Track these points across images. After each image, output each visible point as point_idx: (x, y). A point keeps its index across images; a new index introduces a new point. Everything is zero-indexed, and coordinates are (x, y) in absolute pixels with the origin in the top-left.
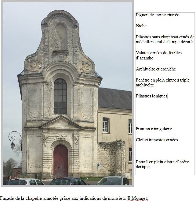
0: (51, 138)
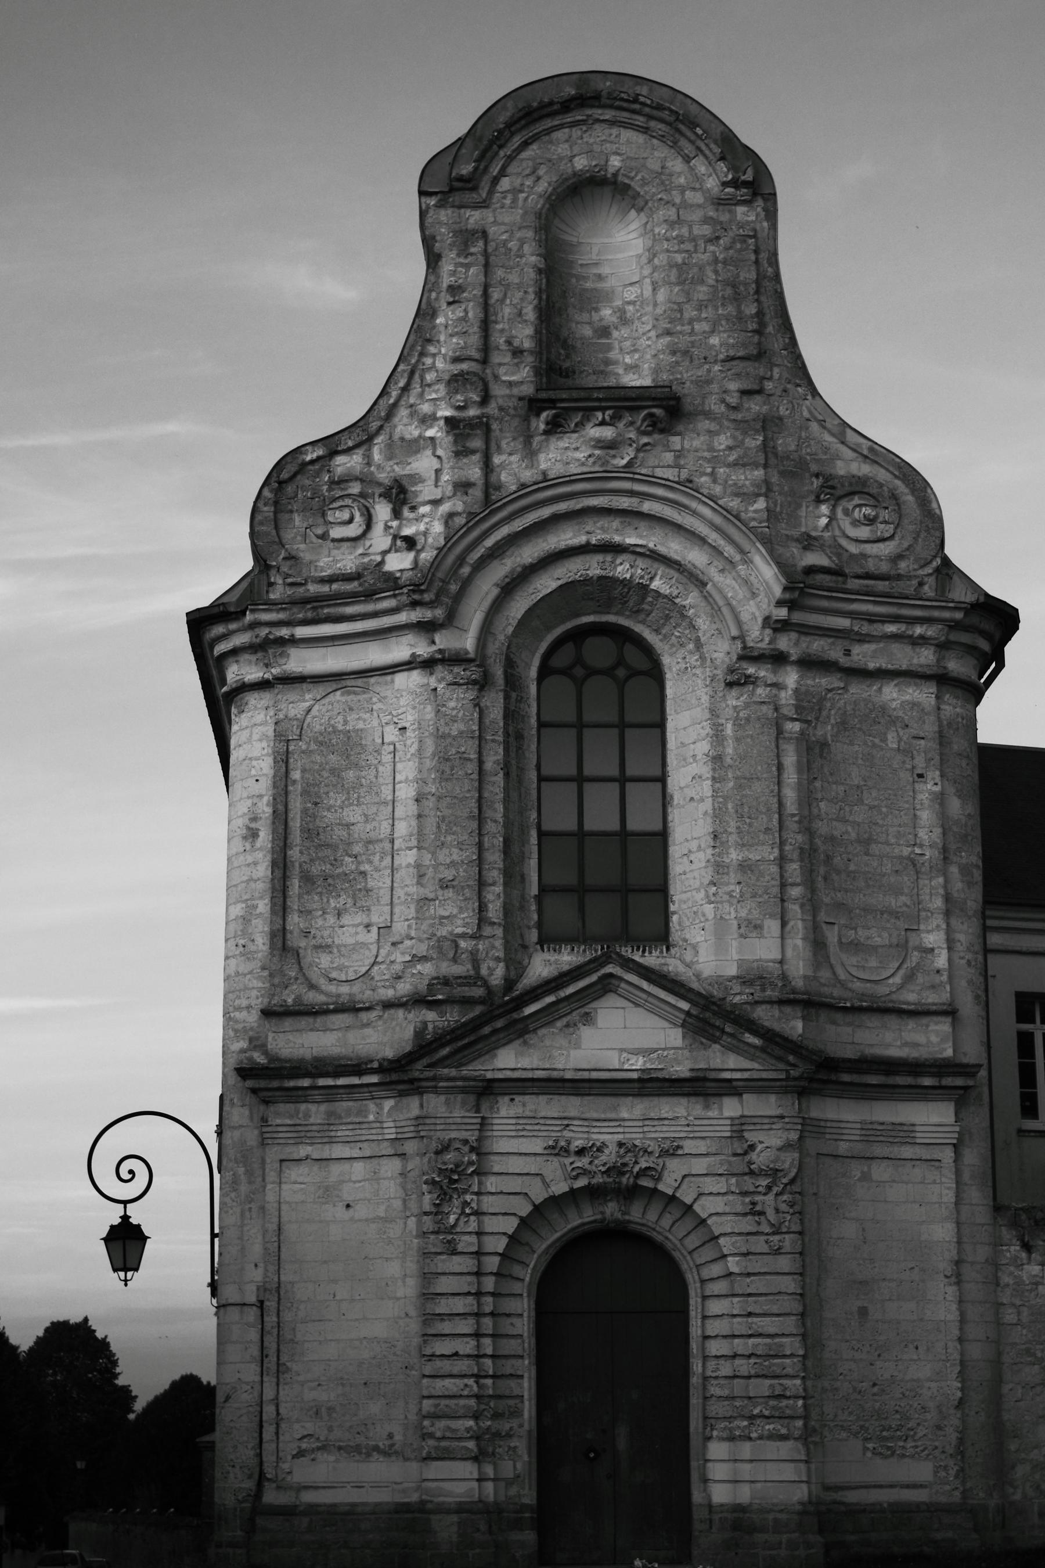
0: (516, 1165)
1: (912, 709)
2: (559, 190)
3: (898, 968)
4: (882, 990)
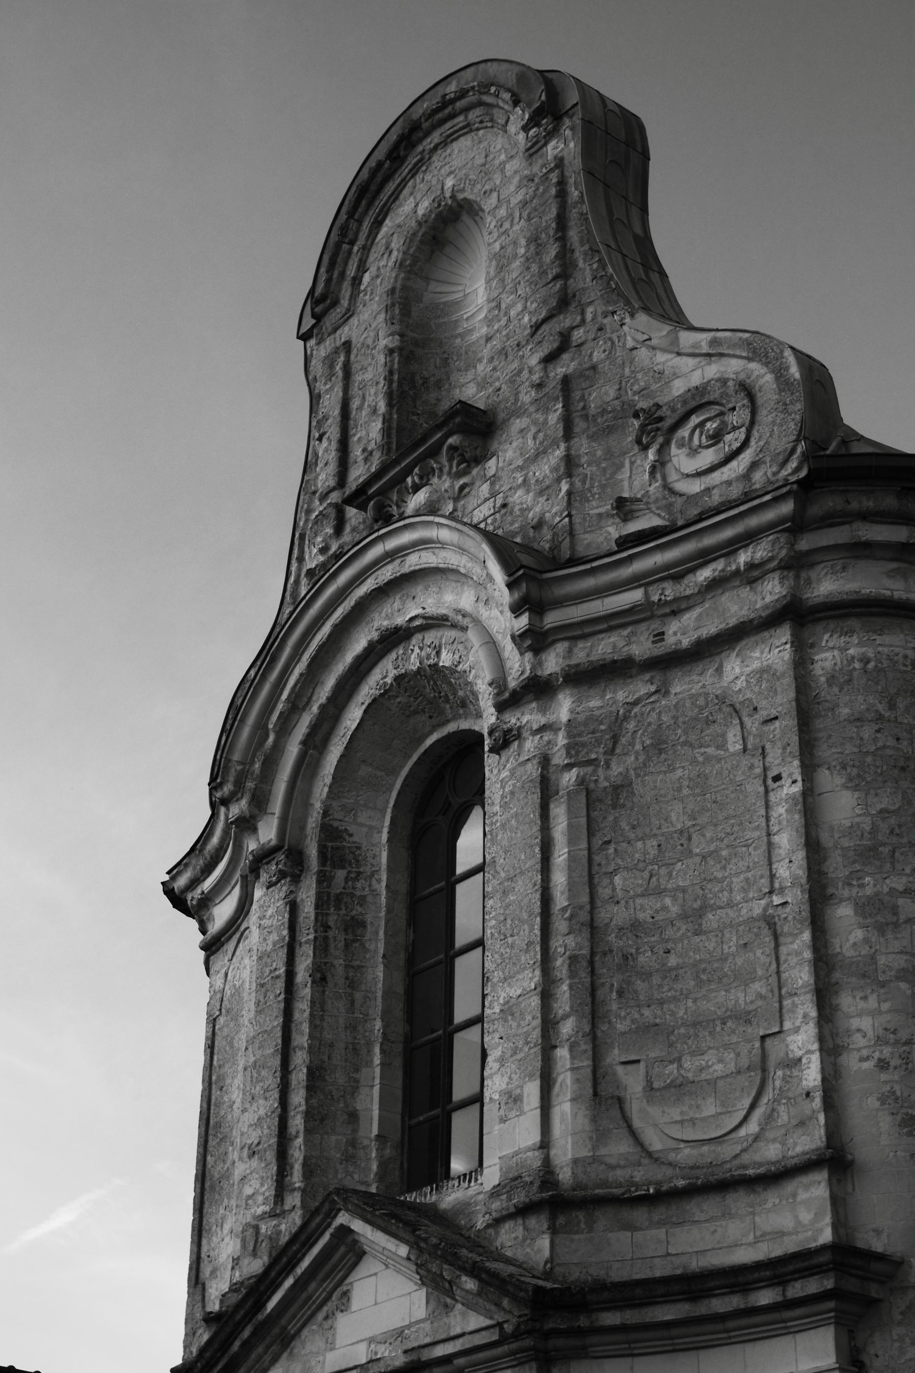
1: (759, 681)
2: (411, 251)
3: (753, 1106)
4: (727, 1151)
